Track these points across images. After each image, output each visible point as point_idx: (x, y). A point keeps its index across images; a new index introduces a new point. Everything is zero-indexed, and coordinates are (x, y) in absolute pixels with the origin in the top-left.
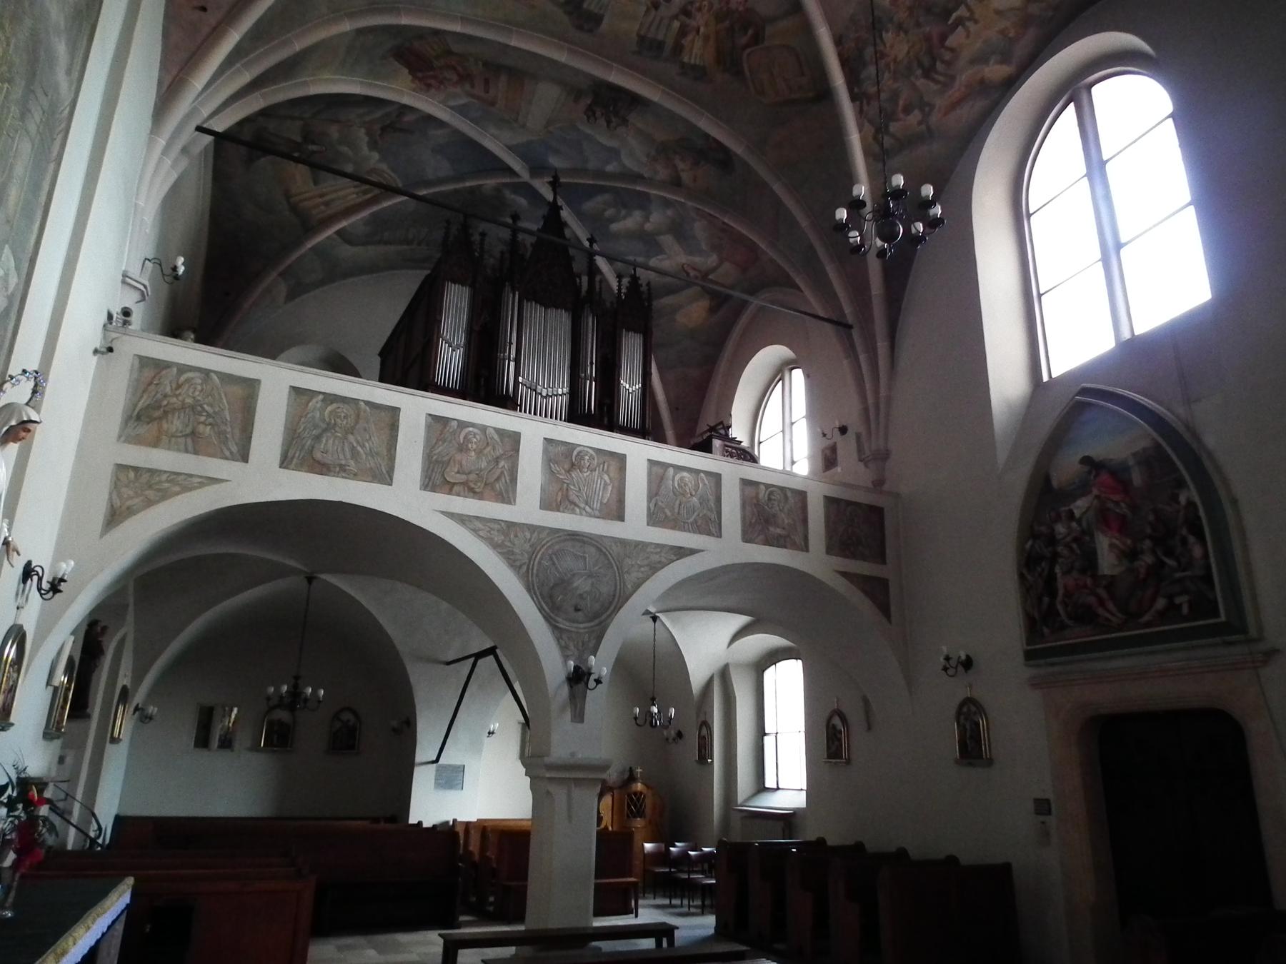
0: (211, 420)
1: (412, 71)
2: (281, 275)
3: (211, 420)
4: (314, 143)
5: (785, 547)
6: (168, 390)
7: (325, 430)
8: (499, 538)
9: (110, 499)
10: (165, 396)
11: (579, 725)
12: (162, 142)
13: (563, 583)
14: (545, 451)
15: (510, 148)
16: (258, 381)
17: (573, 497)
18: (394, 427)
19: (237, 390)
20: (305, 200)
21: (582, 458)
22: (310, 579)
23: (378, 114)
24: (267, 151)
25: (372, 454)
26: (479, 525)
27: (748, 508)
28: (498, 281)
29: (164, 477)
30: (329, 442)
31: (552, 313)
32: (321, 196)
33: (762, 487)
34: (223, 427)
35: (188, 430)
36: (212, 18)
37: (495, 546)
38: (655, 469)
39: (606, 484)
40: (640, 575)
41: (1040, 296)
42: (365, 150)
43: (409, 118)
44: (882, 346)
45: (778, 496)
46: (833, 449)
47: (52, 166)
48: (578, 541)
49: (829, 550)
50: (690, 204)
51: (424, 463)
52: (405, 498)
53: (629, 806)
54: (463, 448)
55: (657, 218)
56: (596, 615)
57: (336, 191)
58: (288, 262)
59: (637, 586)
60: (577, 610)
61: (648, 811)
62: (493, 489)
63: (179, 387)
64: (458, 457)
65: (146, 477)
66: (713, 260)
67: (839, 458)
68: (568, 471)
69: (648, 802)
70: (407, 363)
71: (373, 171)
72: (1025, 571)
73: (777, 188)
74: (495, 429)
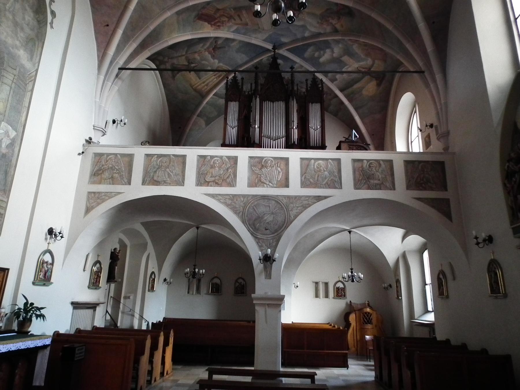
0: (118, 171)
1: (209, 22)
2: (198, 116)
3: (118, 171)
4: (192, 63)
5: (380, 189)
6: (104, 163)
7: (158, 168)
8: (229, 202)
9: (86, 204)
10: (103, 165)
11: (269, 280)
12: (102, 77)
13: (259, 218)
14: (249, 162)
15: (264, 40)
16: (134, 154)
17: (263, 180)
18: (184, 163)
19: (127, 159)
20: (199, 86)
21: (267, 162)
22: (198, 228)
23: (208, 44)
24: (180, 70)
25: (176, 175)
26: (220, 197)
27: (357, 173)
28: (269, 96)
29: (103, 194)
30: (160, 173)
31: (276, 104)
32: (204, 83)
33: (365, 161)
34: (122, 173)
35: (110, 176)
36: (111, 28)
37: (227, 205)
38: (356, 164)
39: (279, 172)
40: (298, 211)
41: (516, 19)
42: (212, 60)
43: (220, 42)
44: (438, 77)
45: (375, 164)
46: (429, 136)
47: (29, 93)
48: (267, 199)
49: (408, 187)
50: (346, 38)
51: (196, 175)
52: (190, 191)
53: (363, 319)
54: (212, 167)
55: (337, 50)
56: (276, 231)
57: (207, 80)
58: (199, 111)
59: (296, 217)
60: (266, 229)
61: (374, 321)
62: (226, 181)
63: (107, 161)
64: (211, 170)
65: (97, 195)
66: (369, 62)
67: (432, 143)
68: (261, 169)
69: (374, 317)
70: (245, 140)
71: (218, 67)
72: (506, 182)
73: (373, 15)
74: (226, 156)
